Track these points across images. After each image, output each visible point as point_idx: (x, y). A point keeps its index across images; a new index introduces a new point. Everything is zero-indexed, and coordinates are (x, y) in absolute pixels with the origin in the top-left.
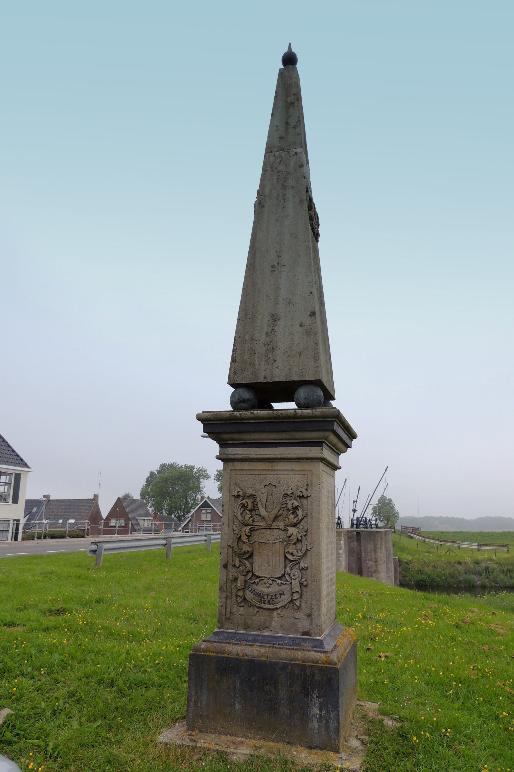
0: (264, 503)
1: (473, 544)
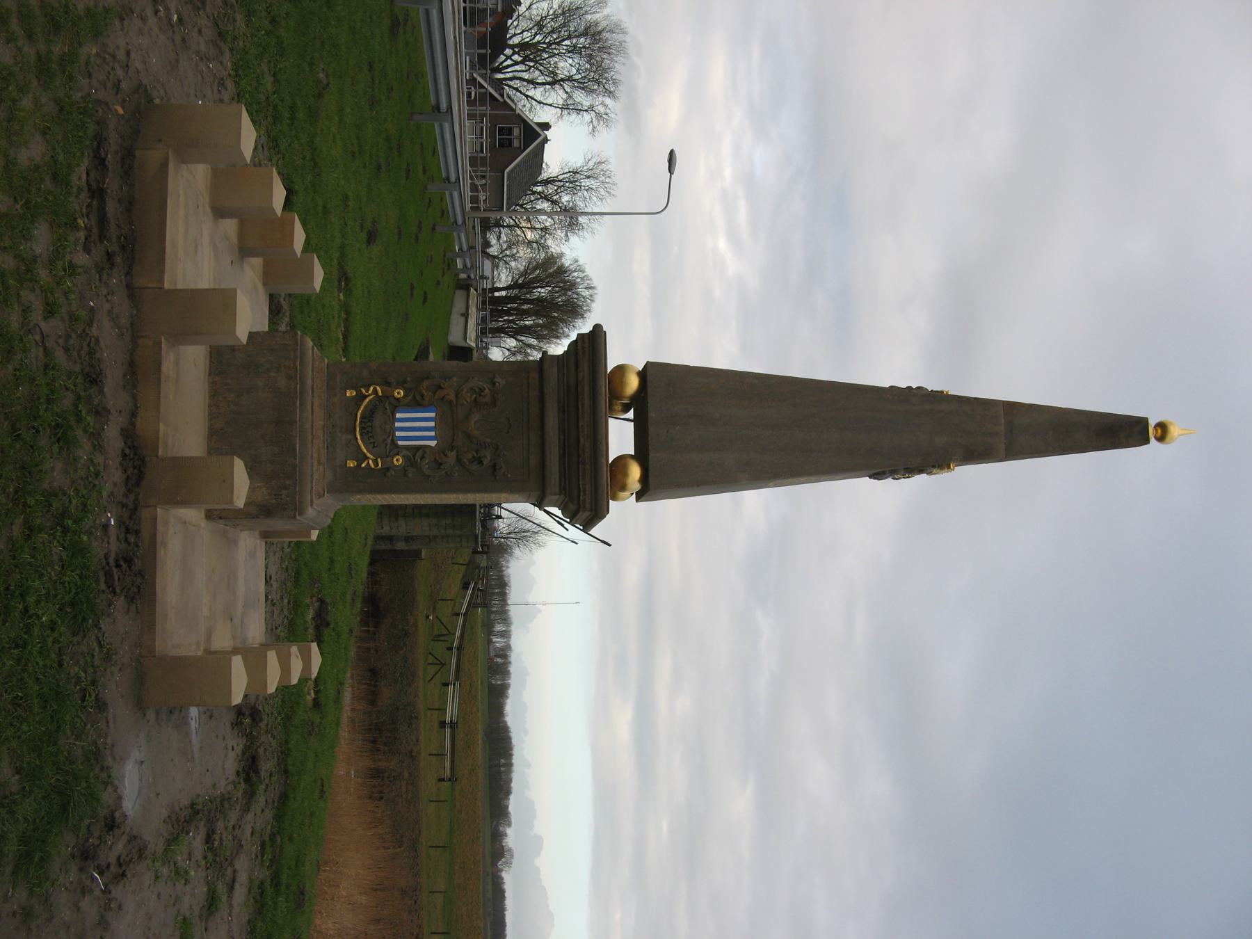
1: (455, 712)
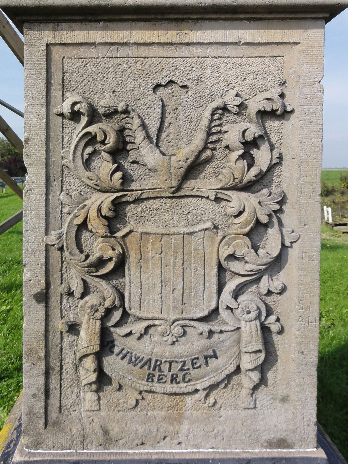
0: (153, 132)
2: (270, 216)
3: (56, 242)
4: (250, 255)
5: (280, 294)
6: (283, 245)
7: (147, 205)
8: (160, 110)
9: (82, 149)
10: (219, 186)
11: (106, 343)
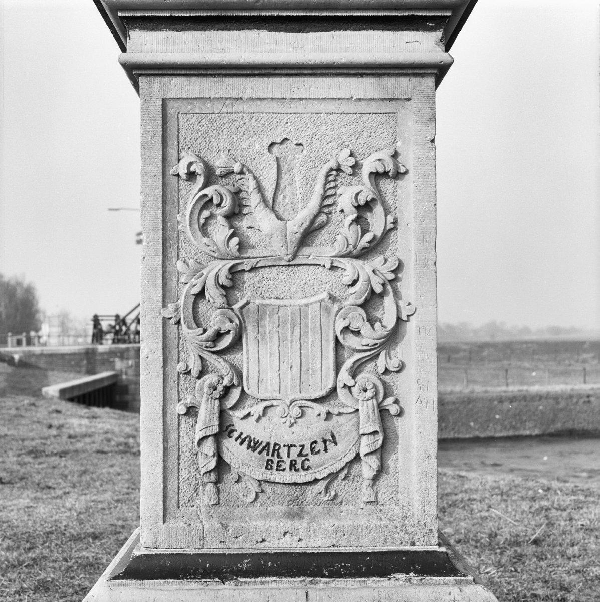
0: (269, 195)
2: (384, 285)
3: (173, 315)
4: (366, 329)
5: (398, 372)
6: (399, 319)
7: (264, 275)
8: (275, 170)
9: (198, 213)
10: (334, 254)
11: (224, 430)
